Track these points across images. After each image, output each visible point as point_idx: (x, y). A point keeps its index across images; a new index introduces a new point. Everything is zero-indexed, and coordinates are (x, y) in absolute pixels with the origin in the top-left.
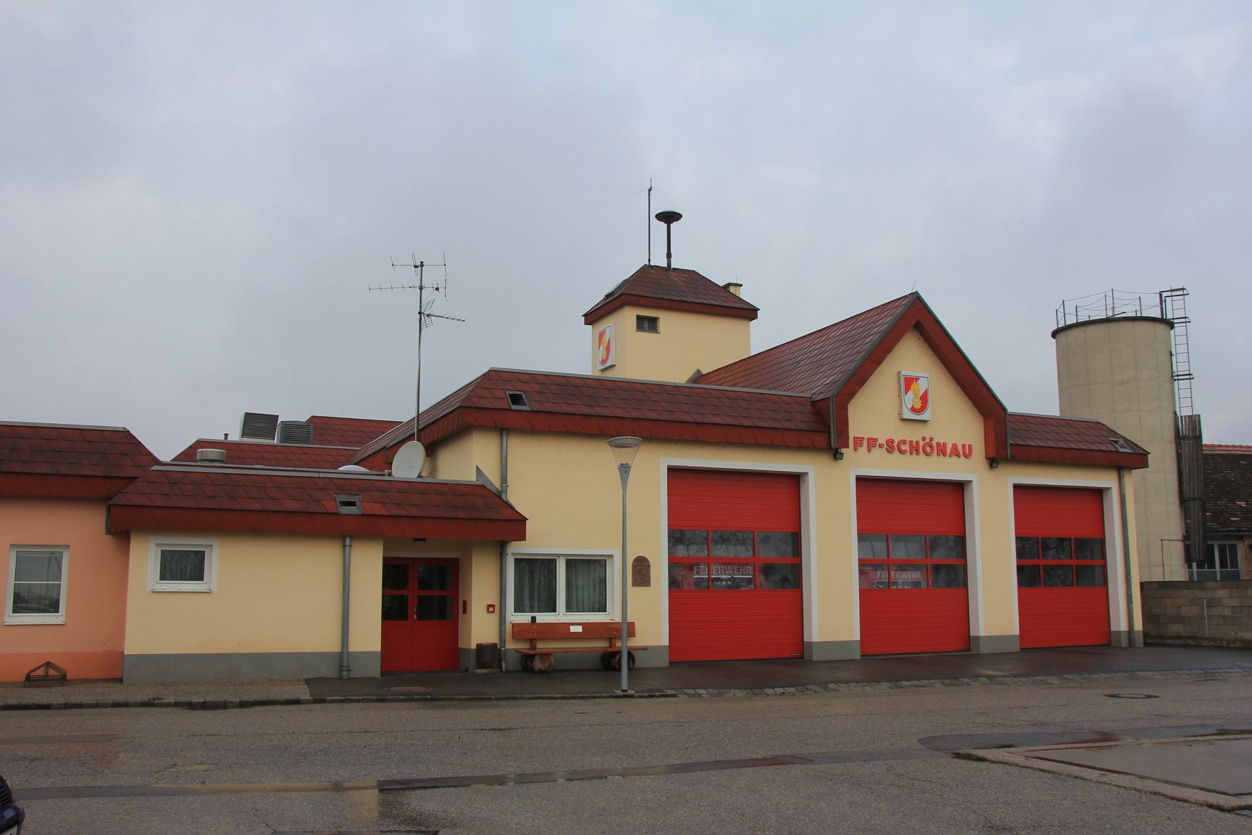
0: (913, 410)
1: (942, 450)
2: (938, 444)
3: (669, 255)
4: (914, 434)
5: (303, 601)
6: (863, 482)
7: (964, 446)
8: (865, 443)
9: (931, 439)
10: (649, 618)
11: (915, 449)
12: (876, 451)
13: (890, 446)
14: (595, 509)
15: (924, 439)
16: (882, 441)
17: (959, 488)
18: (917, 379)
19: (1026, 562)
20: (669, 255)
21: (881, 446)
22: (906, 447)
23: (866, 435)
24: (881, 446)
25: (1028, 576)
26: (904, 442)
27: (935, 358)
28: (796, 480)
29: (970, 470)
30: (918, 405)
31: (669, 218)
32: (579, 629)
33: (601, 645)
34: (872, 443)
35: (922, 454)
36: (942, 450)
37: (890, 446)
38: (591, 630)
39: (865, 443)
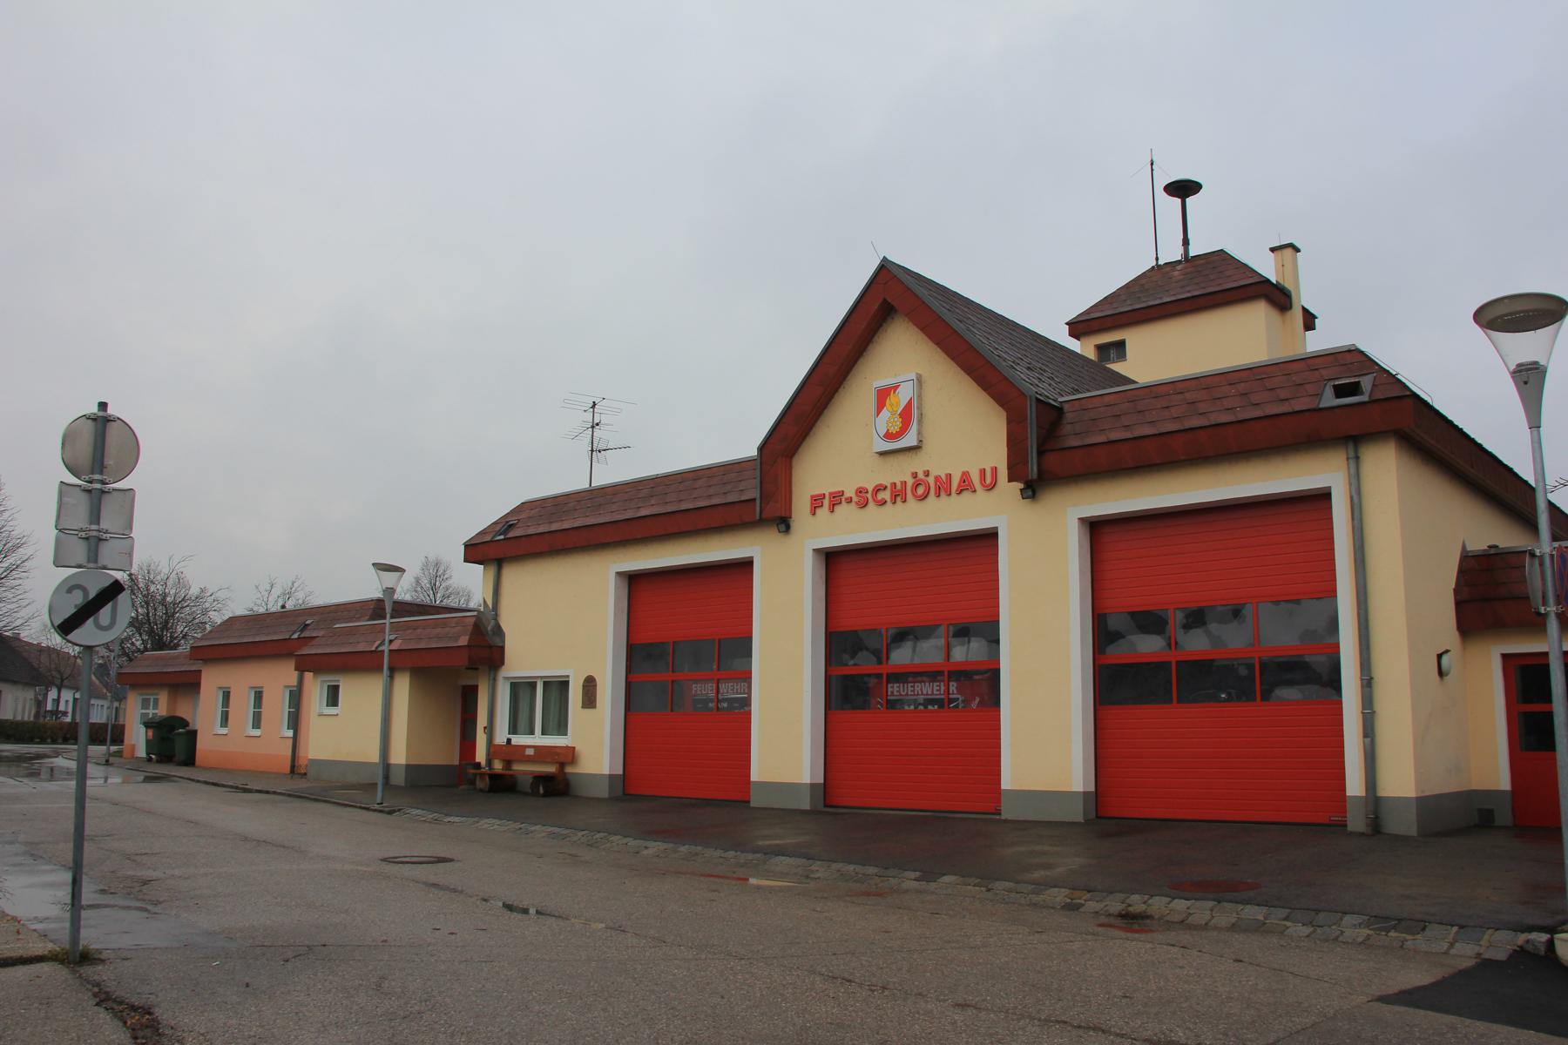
0: (889, 436)
1: (943, 487)
2: (937, 479)
3: (1186, 242)
4: (899, 472)
5: (362, 723)
6: (832, 559)
7: (983, 472)
8: (826, 502)
9: (927, 474)
10: (595, 742)
11: (898, 494)
12: (842, 509)
13: (863, 499)
14: (567, 625)
15: (915, 475)
16: (850, 493)
17: (989, 537)
18: (896, 388)
19: (1118, 652)
20: (1186, 242)
21: (849, 500)
22: (886, 495)
23: (826, 490)
24: (849, 500)
25: (1116, 684)
26: (879, 489)
27: (861, 361)
28: (746, 565)
29: (997, 509)
30: (895, 429)
31: (1183, 189)
32: (530, 752)
33: (551, 769)
34: (836, 499)
35: (871, 504)
36: (943, 487)
37: (863, 499)
38: (543, 753)
39: (826, 502)
